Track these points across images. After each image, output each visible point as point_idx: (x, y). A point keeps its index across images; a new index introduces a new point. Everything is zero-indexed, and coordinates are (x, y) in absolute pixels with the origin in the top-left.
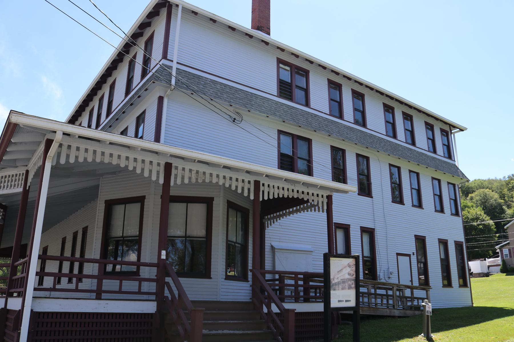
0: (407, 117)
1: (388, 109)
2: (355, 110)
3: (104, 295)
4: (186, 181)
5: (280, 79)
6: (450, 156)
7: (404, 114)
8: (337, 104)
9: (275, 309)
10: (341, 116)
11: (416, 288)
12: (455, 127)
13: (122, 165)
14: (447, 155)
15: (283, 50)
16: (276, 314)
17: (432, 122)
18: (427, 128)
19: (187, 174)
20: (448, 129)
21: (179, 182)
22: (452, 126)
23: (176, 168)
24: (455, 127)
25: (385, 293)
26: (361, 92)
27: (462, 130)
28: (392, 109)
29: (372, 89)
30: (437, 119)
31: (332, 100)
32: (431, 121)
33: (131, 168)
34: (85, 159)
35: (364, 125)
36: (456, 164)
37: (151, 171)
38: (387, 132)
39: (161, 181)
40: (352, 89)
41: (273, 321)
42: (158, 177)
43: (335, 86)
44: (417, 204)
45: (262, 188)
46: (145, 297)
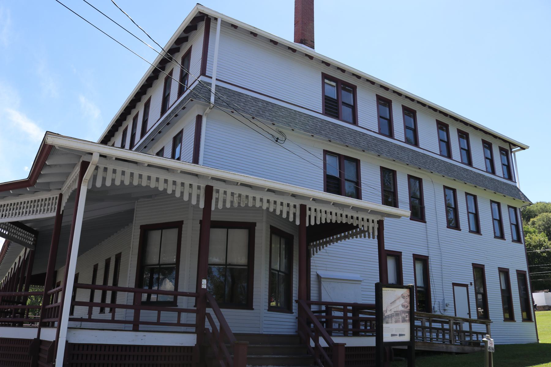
0: (463, 135)
1: (442, 127)
2: (406, 127)
3: (141, 327)
4: (228, 205)
7: (459, 131)
12: (515, 145)
13: (161, 189)
14: (506, 176)
15: (328, 64)
17: (490, 140)
18: (484, 147)
19: (229, 198)
20: (508, 147)
21: (220, 206)
23: (218, 191)
24: (515, 145)
25: (441, 327)
26: (413, 108)
27: (524, 149)
28: (447, 126)
29: (424, 105)
31: (381, 117)
32: (488, 139)
33: (169, 192)
34: (122, 182)
35: (416, 144)
36: (518, 186)
37: (190, 195)
38: (441, 151)
39: (202, 205)
40: (403, 106)
42: (198, 201)
43: (384, 103)
45: (215, 195)
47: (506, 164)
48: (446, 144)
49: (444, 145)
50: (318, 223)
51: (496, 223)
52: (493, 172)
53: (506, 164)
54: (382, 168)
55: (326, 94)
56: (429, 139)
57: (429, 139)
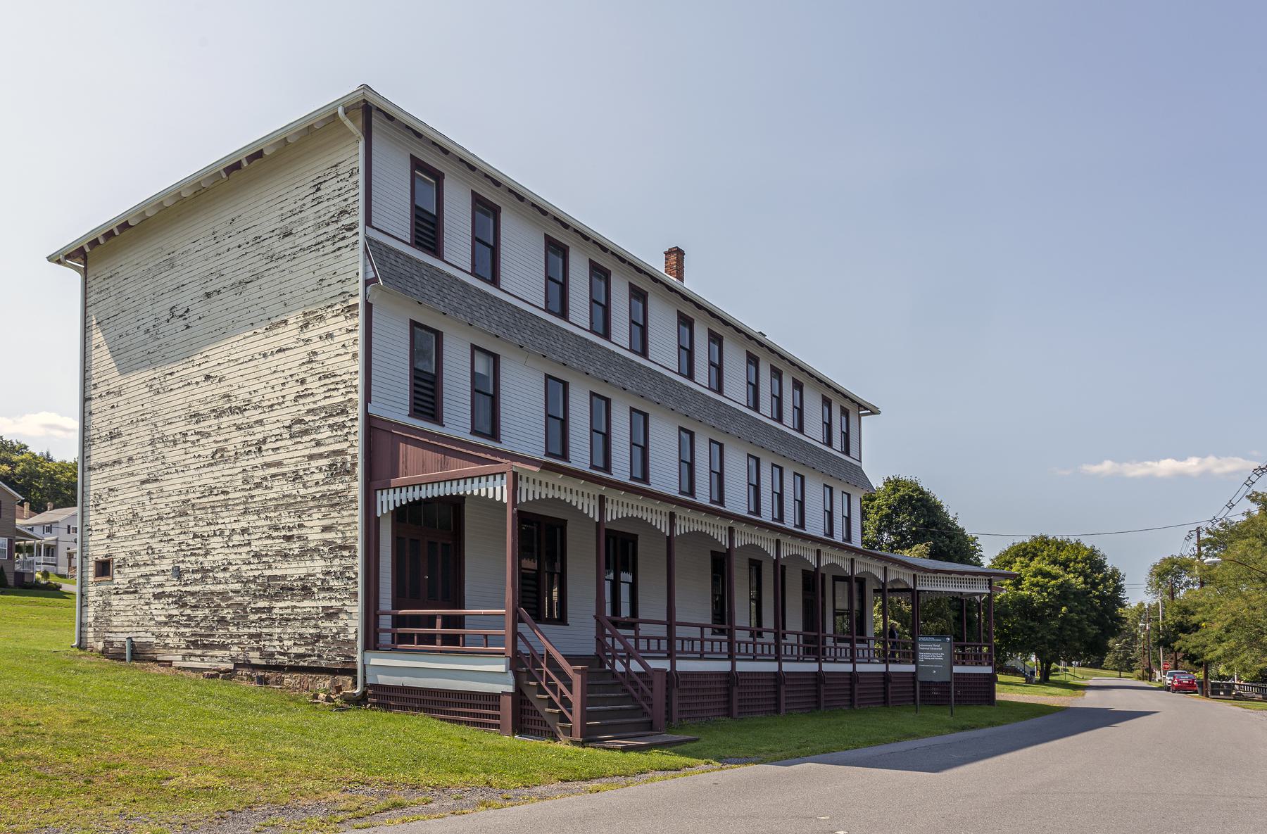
1: (556, 249)
5: (417, 207)
6: (847, 451)
7: (477, 200)
8: (558, 286)
9: (619, 667)
10: (564, 314)
11: (637, 633)
14: (714, 386)
16: (637, 673)
17: (832, 395)
18: (748, 362)
22: (861, 406)
25: (784, 664)
26: (494, 201)
27: (872, 413)
28: (438, 177)
30: (622, 259)
31: (550, 278)
38: (547, 302)
41: (634, 683)
44: (639, 476)
46: (372, 621)
47: (717, 362)
48: (687, 353)
49: (637, 330)
50: (531, 498)
51: (685, 466)
52: (690, 376)
53: (717, 362)
54: (414, 324)
55: (418, 203)
56: (523, 276)
57: (523, 276)
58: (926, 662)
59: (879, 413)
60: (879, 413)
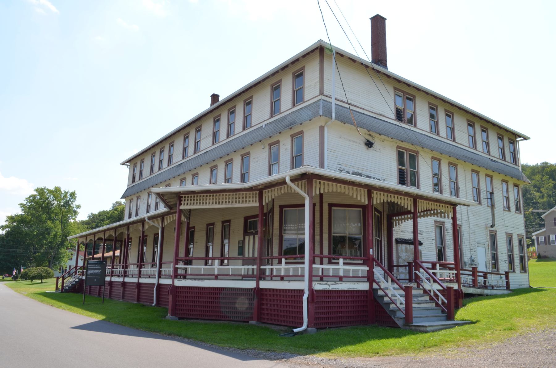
58: (91, 275)
59: (529, 138)
60: (529, 138)
